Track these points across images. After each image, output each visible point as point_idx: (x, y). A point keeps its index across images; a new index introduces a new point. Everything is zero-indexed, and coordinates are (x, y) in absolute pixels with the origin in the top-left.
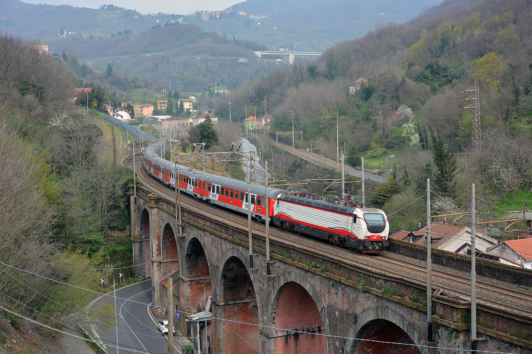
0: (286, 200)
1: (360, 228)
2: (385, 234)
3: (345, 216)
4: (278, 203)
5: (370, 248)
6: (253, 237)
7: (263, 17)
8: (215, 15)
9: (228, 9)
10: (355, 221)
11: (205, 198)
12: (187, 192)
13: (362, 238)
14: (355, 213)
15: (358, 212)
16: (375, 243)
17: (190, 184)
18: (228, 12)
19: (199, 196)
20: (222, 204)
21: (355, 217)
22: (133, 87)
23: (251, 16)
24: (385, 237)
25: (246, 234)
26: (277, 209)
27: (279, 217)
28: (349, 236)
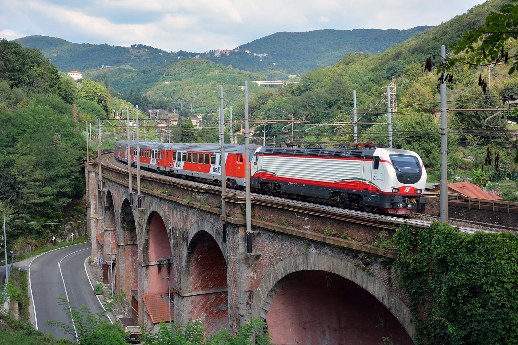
0: (268, 153)
1: (386, 174)
2: (422, 184)
3: (360, 161)
4: (257, 160)
5: (401, 205)
6: (132, 177)
7: (265, 55)
8: (226, 53)
9: (236, 49)
10: (376, 167)
11: (168, 170)
12: (150, 167)
13: (390, 190)
14: (375, 154)
15: (379, 152)
16: (407, 199)
17: (153, 157)
18: (236, 51)
19: (162, 169)
20: (189, 173)
21: (377, 161)
22: (151, 107)
23: (255, 54)
24: (421, 190)
25: (126, 175)
26: (256, 166)
27: (259, 177)
28: (366, 189)
